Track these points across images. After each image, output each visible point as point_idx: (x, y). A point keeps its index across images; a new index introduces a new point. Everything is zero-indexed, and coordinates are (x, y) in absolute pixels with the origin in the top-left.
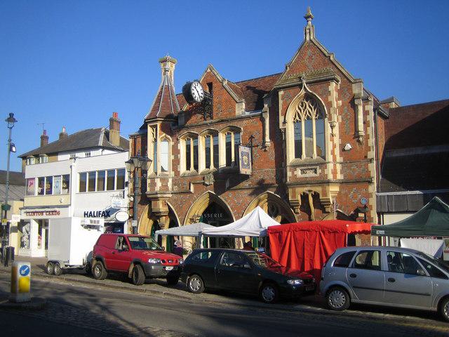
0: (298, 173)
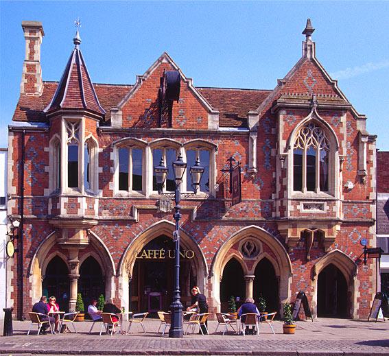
0: (301, 207)
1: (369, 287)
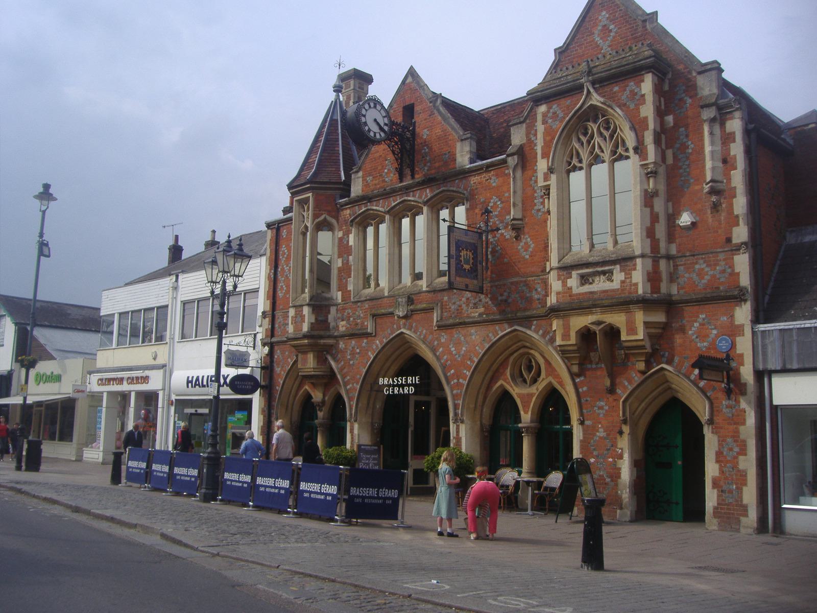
1: (739, 454)
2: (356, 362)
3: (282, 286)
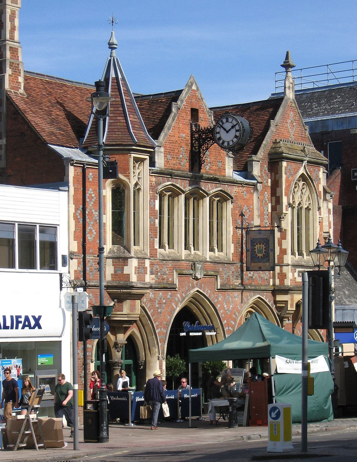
2: (163, 311)
3: (91, 230)
